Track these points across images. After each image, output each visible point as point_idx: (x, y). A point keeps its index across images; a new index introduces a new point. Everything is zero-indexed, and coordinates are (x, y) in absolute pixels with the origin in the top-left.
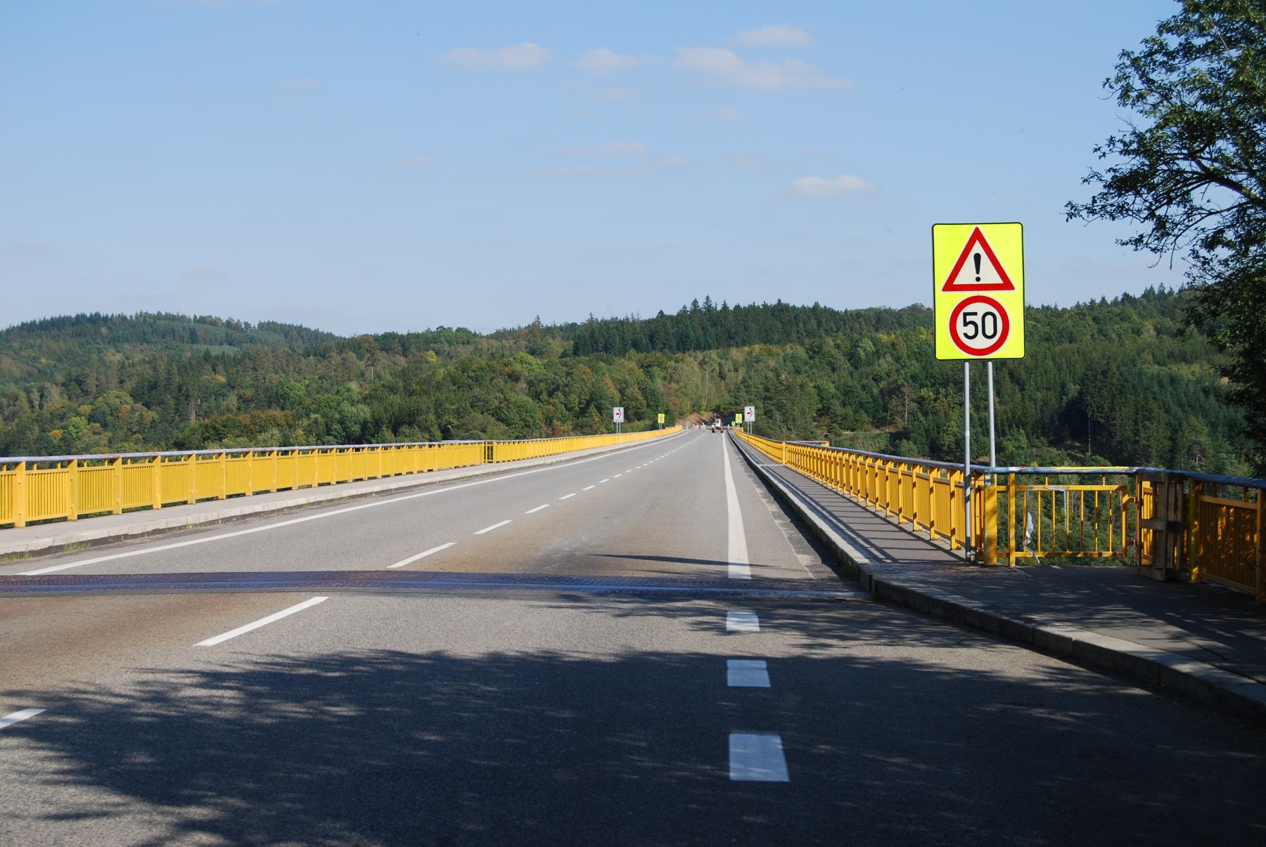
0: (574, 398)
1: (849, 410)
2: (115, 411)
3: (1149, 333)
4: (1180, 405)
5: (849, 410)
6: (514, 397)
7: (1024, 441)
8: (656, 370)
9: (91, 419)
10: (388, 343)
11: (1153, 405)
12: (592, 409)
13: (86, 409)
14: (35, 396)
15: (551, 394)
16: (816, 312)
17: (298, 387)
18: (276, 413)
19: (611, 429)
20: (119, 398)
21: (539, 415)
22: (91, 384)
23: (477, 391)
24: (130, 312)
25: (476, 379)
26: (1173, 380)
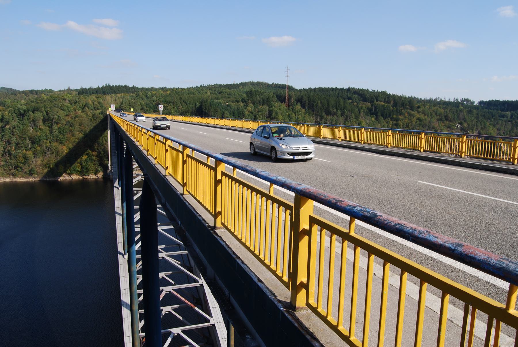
1: (148, 108)
3: (209, 93)
5: (148, 108)
6: (65, 104)
10: (32, 92)
12: (86, 107)
15: (75, 103)
17: (8, 102)
19: (131, 112)
23: (55, 102)
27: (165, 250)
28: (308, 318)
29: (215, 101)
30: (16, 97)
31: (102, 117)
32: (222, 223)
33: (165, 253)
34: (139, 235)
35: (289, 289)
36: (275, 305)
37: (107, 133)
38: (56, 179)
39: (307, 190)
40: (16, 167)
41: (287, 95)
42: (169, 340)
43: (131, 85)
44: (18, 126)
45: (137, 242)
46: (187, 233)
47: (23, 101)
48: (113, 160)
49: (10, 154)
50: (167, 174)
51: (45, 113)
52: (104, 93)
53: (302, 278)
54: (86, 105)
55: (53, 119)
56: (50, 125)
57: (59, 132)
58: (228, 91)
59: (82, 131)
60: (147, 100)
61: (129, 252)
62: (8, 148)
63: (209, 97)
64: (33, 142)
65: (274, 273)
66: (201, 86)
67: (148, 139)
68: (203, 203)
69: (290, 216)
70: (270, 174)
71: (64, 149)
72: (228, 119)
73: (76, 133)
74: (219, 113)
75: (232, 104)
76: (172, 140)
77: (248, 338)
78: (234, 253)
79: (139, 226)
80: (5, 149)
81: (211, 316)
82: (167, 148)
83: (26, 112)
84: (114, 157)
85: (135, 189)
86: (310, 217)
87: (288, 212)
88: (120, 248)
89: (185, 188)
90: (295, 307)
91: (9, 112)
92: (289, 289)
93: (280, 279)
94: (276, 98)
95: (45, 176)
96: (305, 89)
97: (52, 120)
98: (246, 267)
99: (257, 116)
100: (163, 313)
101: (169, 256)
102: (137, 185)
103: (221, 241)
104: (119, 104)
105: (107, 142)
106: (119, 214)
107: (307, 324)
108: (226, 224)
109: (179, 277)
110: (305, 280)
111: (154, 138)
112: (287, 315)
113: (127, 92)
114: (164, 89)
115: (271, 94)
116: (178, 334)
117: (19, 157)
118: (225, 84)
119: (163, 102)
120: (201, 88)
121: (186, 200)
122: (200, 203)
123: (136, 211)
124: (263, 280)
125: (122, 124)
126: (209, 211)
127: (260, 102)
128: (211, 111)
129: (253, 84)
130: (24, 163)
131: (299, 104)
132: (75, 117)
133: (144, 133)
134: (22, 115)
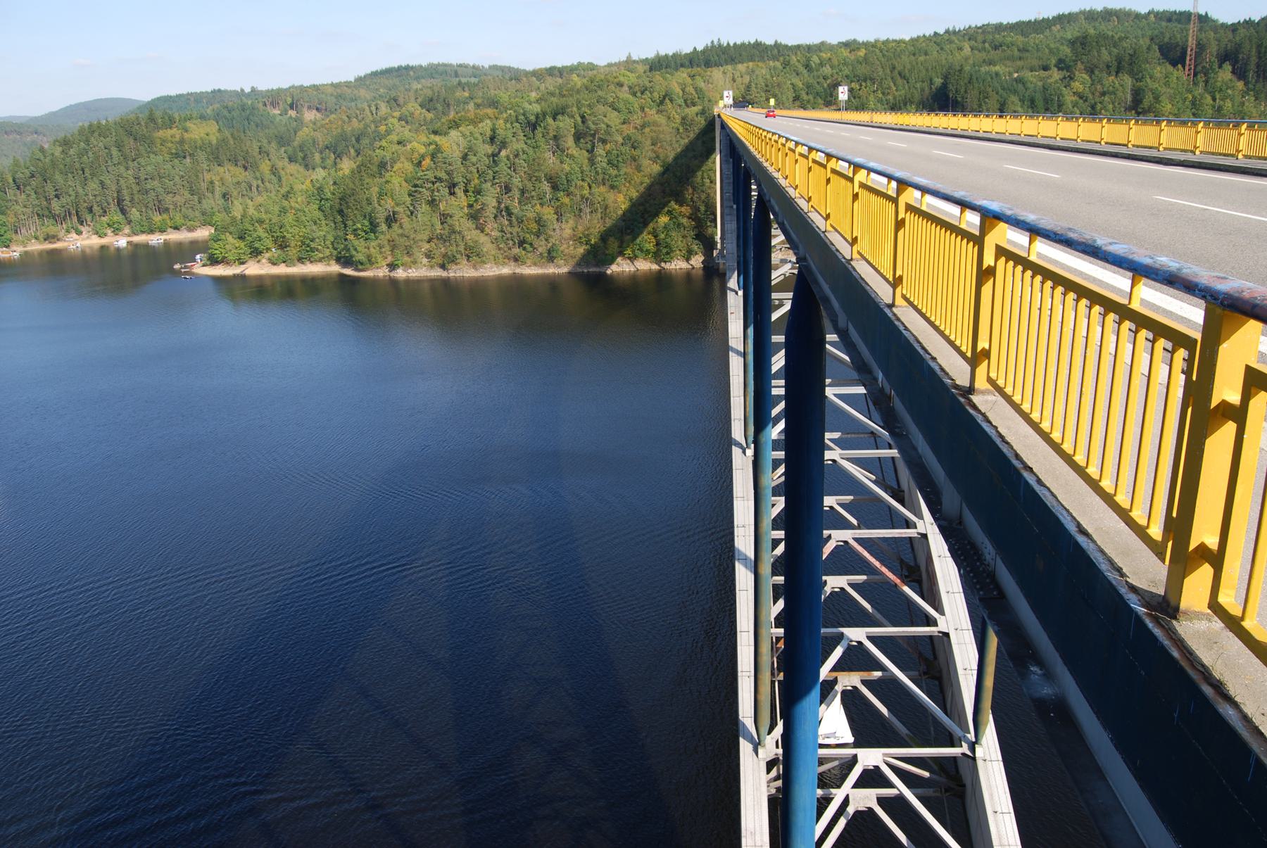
0: (656, 95)
1: (811, 97)
5: (811, 97)
6: (621, 95)
9: (400, 119)
10: (551, 71)
12: (667, 101)
13: (397, 114)
14: (373, 108)
17: (504, 97)
18: (490, 111)
20: (413, 107)
21: (636, 105)
22: (401, 101)
23: (600, 93)
24: (424, 64)
27: (840, 443)
28: (1212, 642)
29: (984, 69)
30: (518, 86)
31: (701, 122)
32: (990, 380)
33: (839, 451)
34: (782, 405)
35: (1163, 561)
36: (1120, 596)
37: (714, 162)
38: (602, 270)
39: (1246, 295)
40: (522, 243)
41: (1191, 43)
42: (838, 652)
43: (769, 41)
44: (524, 152)
45: (776, 421)
46: (897, 404)
47: (533, 95)
48: (727, 226)
49: (510, 214)
50: (856, 256)
51: (579, 119)
52: (708, 64)
53: (1205, 533)
54: (667, 97)
55: (596, 131)
56: (589, 147)
57: (609, 163)
58: (1020, 39)
59: (658, 157)
60: (812, 77)
61: (756, 442)
62: (506, 201)
63: (967, 59)
64: (555, 187)
65: (1124, 515)
66: (947, 32)
67: (810, 169)
68: (942, 328)
69: (1183, 377)
70: (1135, 249)
71: (620, 202)
72: (1016, 114)
73: (646, 163)
74: (993, 102)
75: (1028, 75)
76: (870, 170)
77: (1034, 673)
78: (1017, 456)
79: (782, 382)
80: (499, 203)
81: (942, 613)
82: (856, 190)
83: (540, 117)
84: (727, 218)
85: (774, 296)
86: (1248, 368)
87: (1182, 353)
88: (737, 432)
89: (898, 290)
90: (1177, 609)
91: (506, 121)
92: (1163, 561)
93: (1141, 532)
94: (1158, 54)
95: (578, 264)
96: (1249, 23)
97: (593, 136)
98: (1048, 494)
99: (1099, 106)
100: (828, 589)
101: (848, 459)
102: (781, 287)
103: (985, 425)
104: (742, 88)
105: (713, 182)
106: (737, 352)
107: (1206, 657)
108: (1001, 382)
109: (869, 511)
110: (1212, 542)
111: (825, 167)
112: (1150, 625)
113: (762, 59)
114: (851, 45)
115: (1144, 42)
116: (860, 643)
117: (528, 220)
118: (1013, 20)
119: (849, 79)
120: (946, 37)
121: (898, 319)
122: (936, 328)
123: (777, 347)
124: (1090, 531)
125: (749, 136)
126: (957, 349)
127: (1108, 67)
128: (972, 98)
129: (1090, 16)
130: (538, 235)
131: (1228, 67)
132: (643, 126)
133: (801, 155)
134: (532, 126)
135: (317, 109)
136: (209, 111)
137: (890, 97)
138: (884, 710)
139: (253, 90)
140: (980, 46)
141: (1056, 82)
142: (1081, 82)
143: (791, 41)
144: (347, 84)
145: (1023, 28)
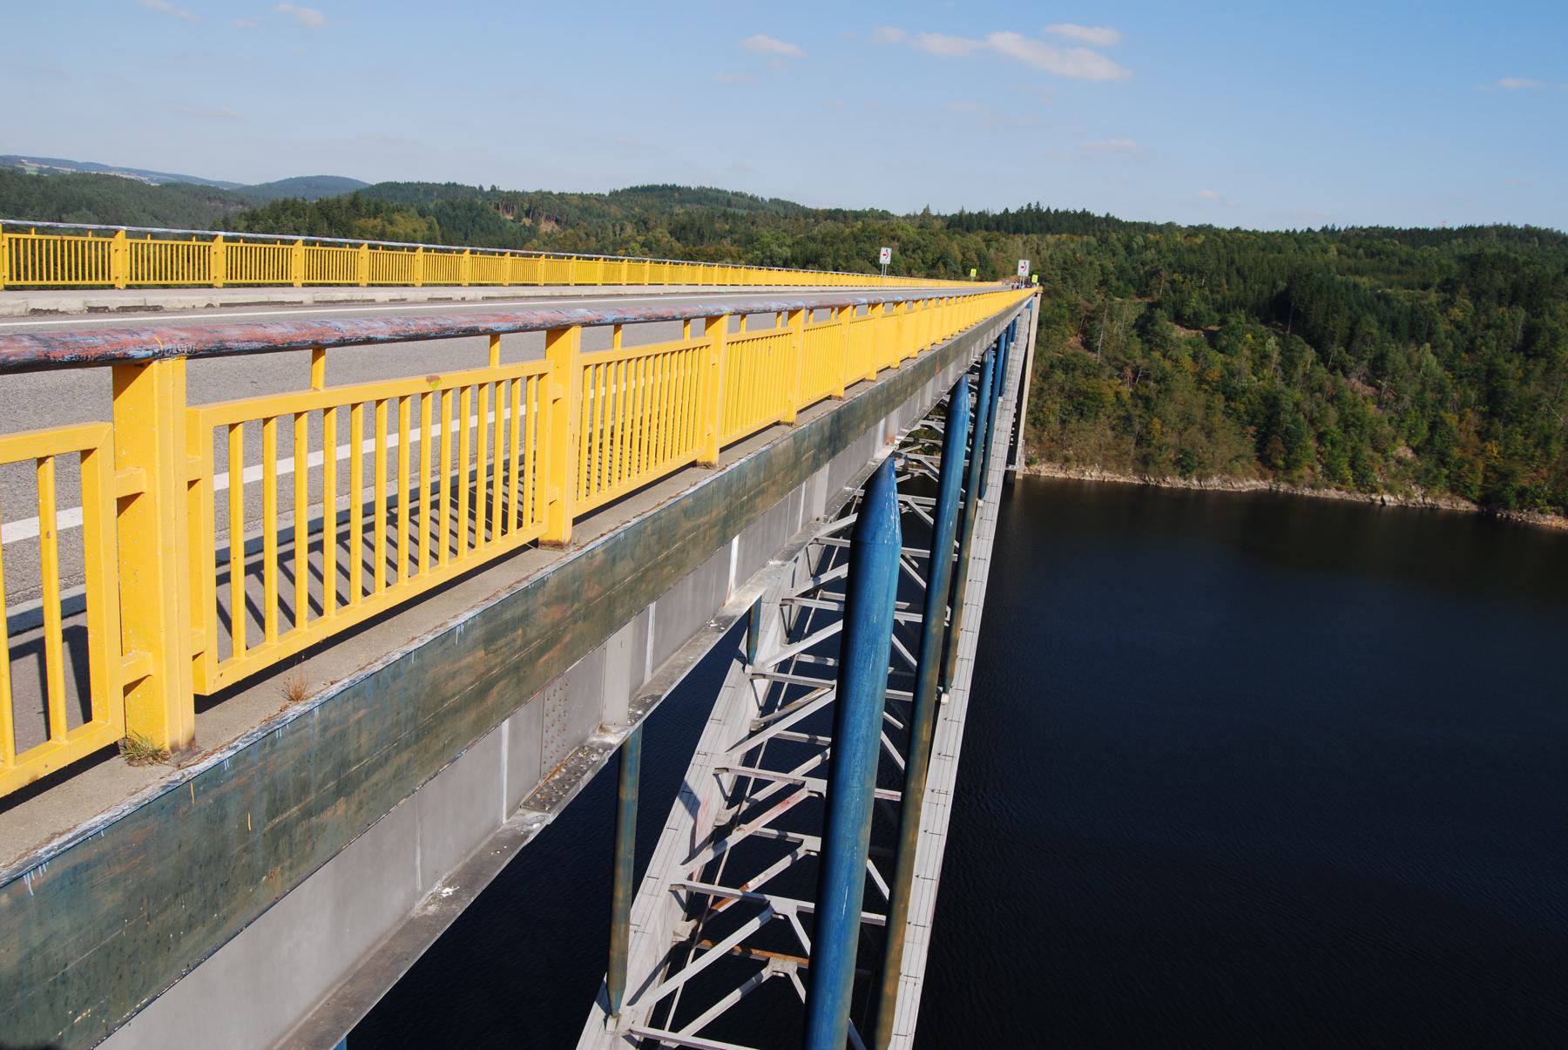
0: (929, 256)
1: (1121, 284)
2: (658, 241)
4: (1360, 305)
5: (1121, 284)
7: (1243, 317)
8: (994, 244)
11: (1342, 303)
12: (940, 264)
13: (641, 239)
16: (1109, 220)
19: (877, 268)
21: (903, 265)
22: (651, 223)
25: (869, 238)
26: (1355, 286)
43: (1099, 213)
58: (1405, 249)
66: (1324, 230)
99: (1479, 341)
118: (1407, 226)
127: (1500, 295)
135: (557, 221)
136: (431, 206)
137: (1219, 297)
138: (735, 997)
139: (493, 189)
140: (1351, 251)
141: (1430, 305)
142: (1463, 308)
143: (1126, 216)
144: (599, 197)
145: (1417, 237)
